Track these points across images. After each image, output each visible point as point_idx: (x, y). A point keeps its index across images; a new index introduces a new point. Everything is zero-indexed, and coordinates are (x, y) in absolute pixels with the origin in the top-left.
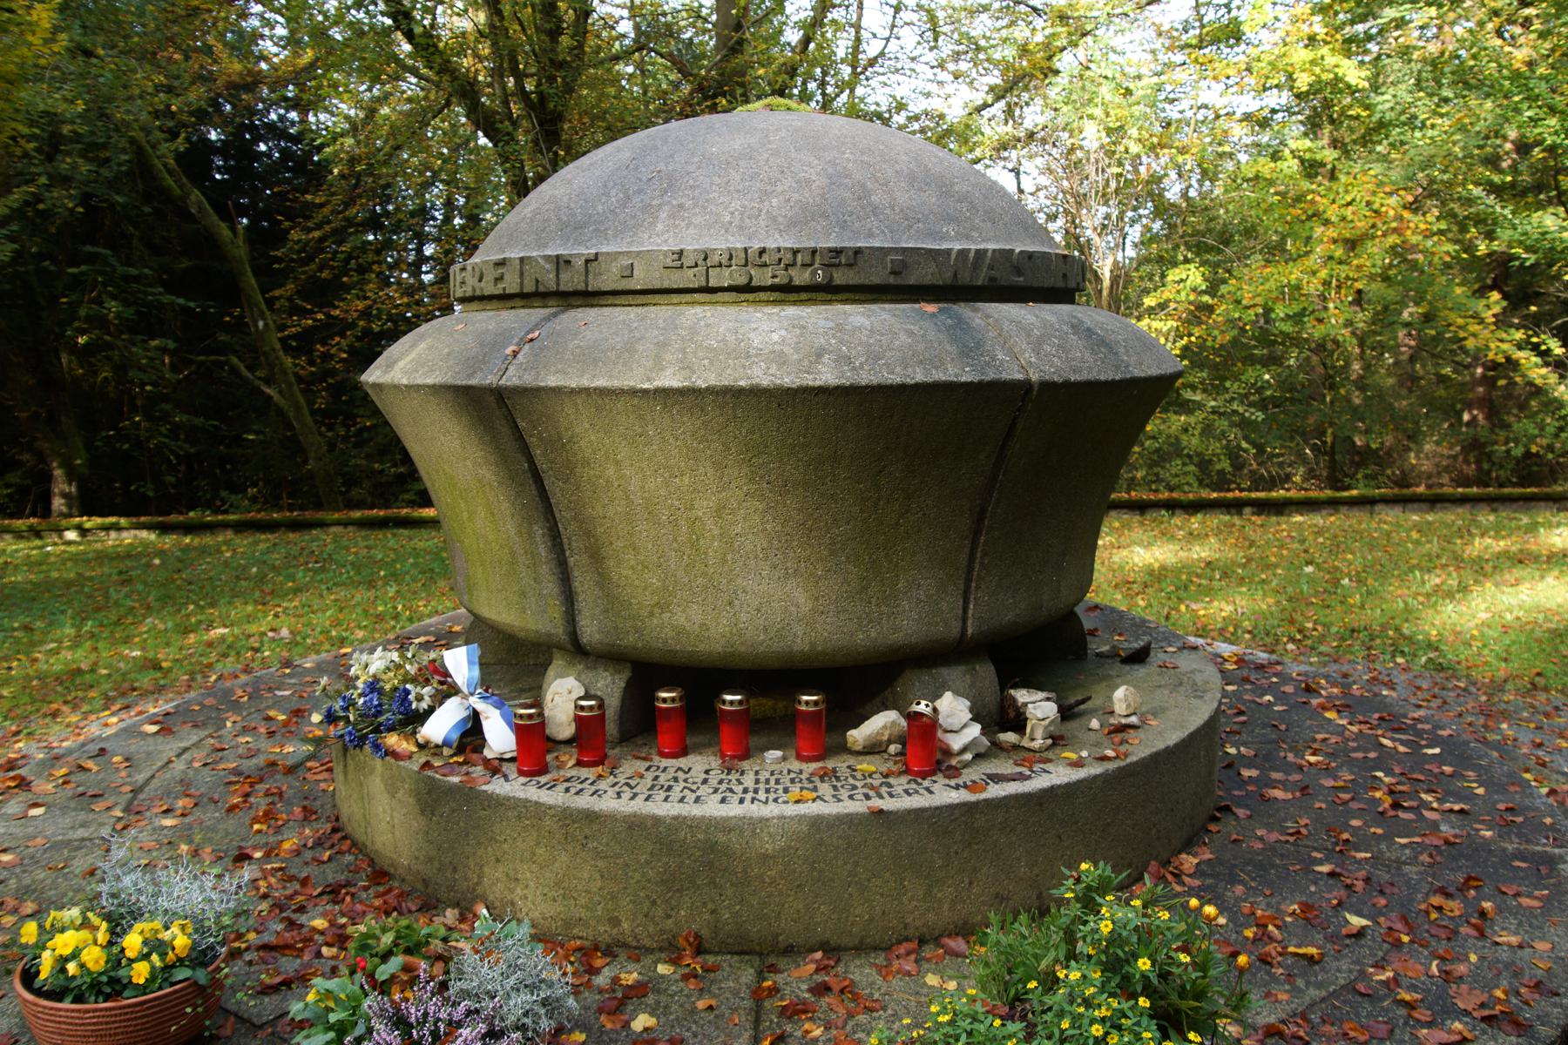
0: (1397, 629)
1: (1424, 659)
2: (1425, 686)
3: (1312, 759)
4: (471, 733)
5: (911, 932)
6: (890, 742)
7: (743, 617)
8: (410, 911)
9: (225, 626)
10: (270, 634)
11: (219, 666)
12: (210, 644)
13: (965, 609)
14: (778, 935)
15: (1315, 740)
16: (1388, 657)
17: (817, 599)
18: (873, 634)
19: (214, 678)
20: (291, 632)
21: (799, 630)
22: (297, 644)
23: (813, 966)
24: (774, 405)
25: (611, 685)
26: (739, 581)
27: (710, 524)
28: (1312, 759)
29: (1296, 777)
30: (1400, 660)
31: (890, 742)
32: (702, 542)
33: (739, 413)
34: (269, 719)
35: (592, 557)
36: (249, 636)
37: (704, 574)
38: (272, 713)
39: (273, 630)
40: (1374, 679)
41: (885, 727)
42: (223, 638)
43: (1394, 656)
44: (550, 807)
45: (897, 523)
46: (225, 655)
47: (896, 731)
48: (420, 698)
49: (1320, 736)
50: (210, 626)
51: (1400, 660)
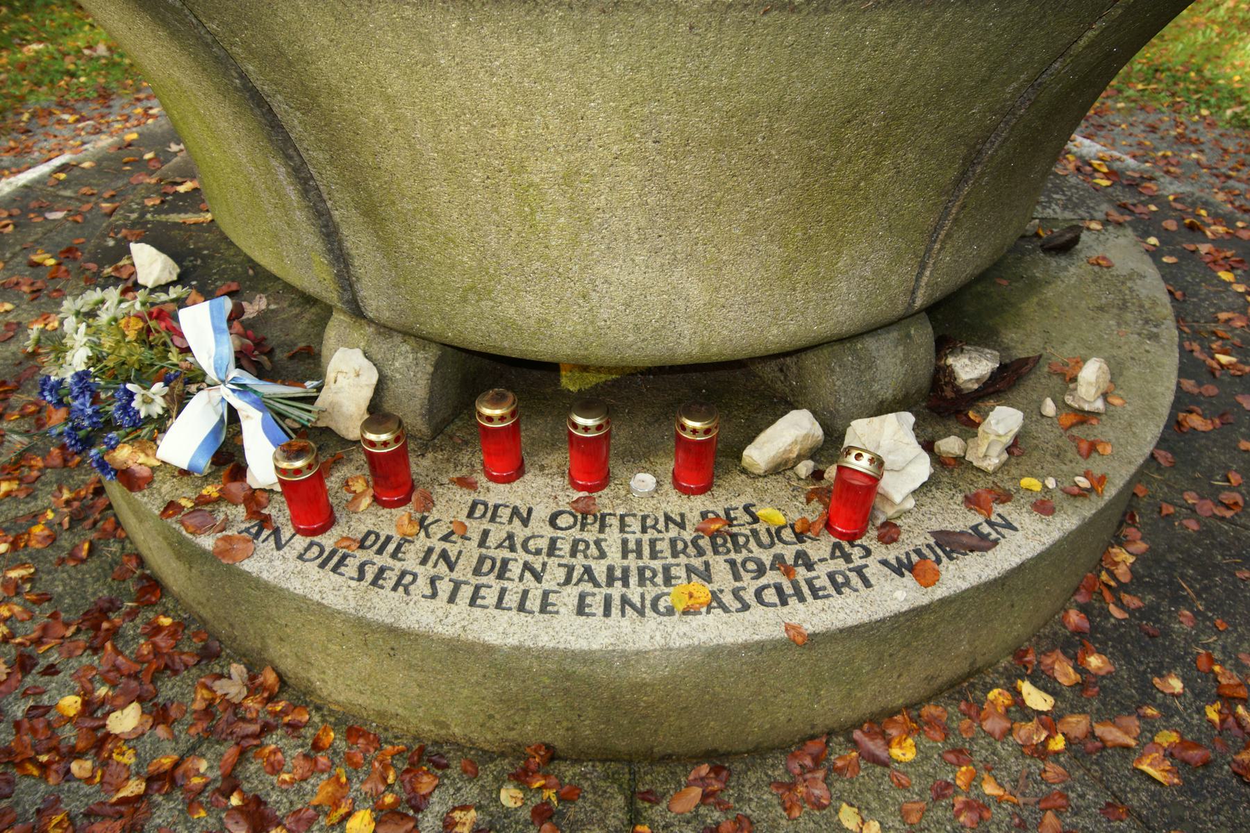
0: (1199, 71)
1: (1229, 113)
2: (1231, 148)
3: (1224, 359)
4: (227, 455)
5: (817, 730)
6: (800, 458)
7: (604, 314)
8: (187, 667)
9: (40, 41)
10: (87, 52)
11: (32, 99)
12: (22, 67)
13: (919, 275)
14: (652, 747)
15: (1217, 320)
16: (1193, 107)
17: (717, 290)
18: (792, 328)
19: (26, 117)
20: (109, 49)
21: (686, 329)
22: (115, 64)
23: (696, 792)
24: (683, 28)
25: (414, 376)
26: (599, 269)
27: (553, 193)
28: (1224, 359)
29: (1211, 390)
30: (1204, 112)
31: (800, 458)
32: (539, 216)
33: (613, 39)
34: (35, 265)
35: (365, 214)
36: (65, 55)
37: (543, 258)
38: (36, 258)
39: (90, 47)
40: (1181, 136)
41: (795, 442)
42: (37, 60)
43: (1198, 107)
44: (339, 612)
45: (856, 187)
46: (38, 84)
47: (809, 444)
48: (148, 401)
49: (1223, 316)
50: (24, 43)
51: (1204, 112)
